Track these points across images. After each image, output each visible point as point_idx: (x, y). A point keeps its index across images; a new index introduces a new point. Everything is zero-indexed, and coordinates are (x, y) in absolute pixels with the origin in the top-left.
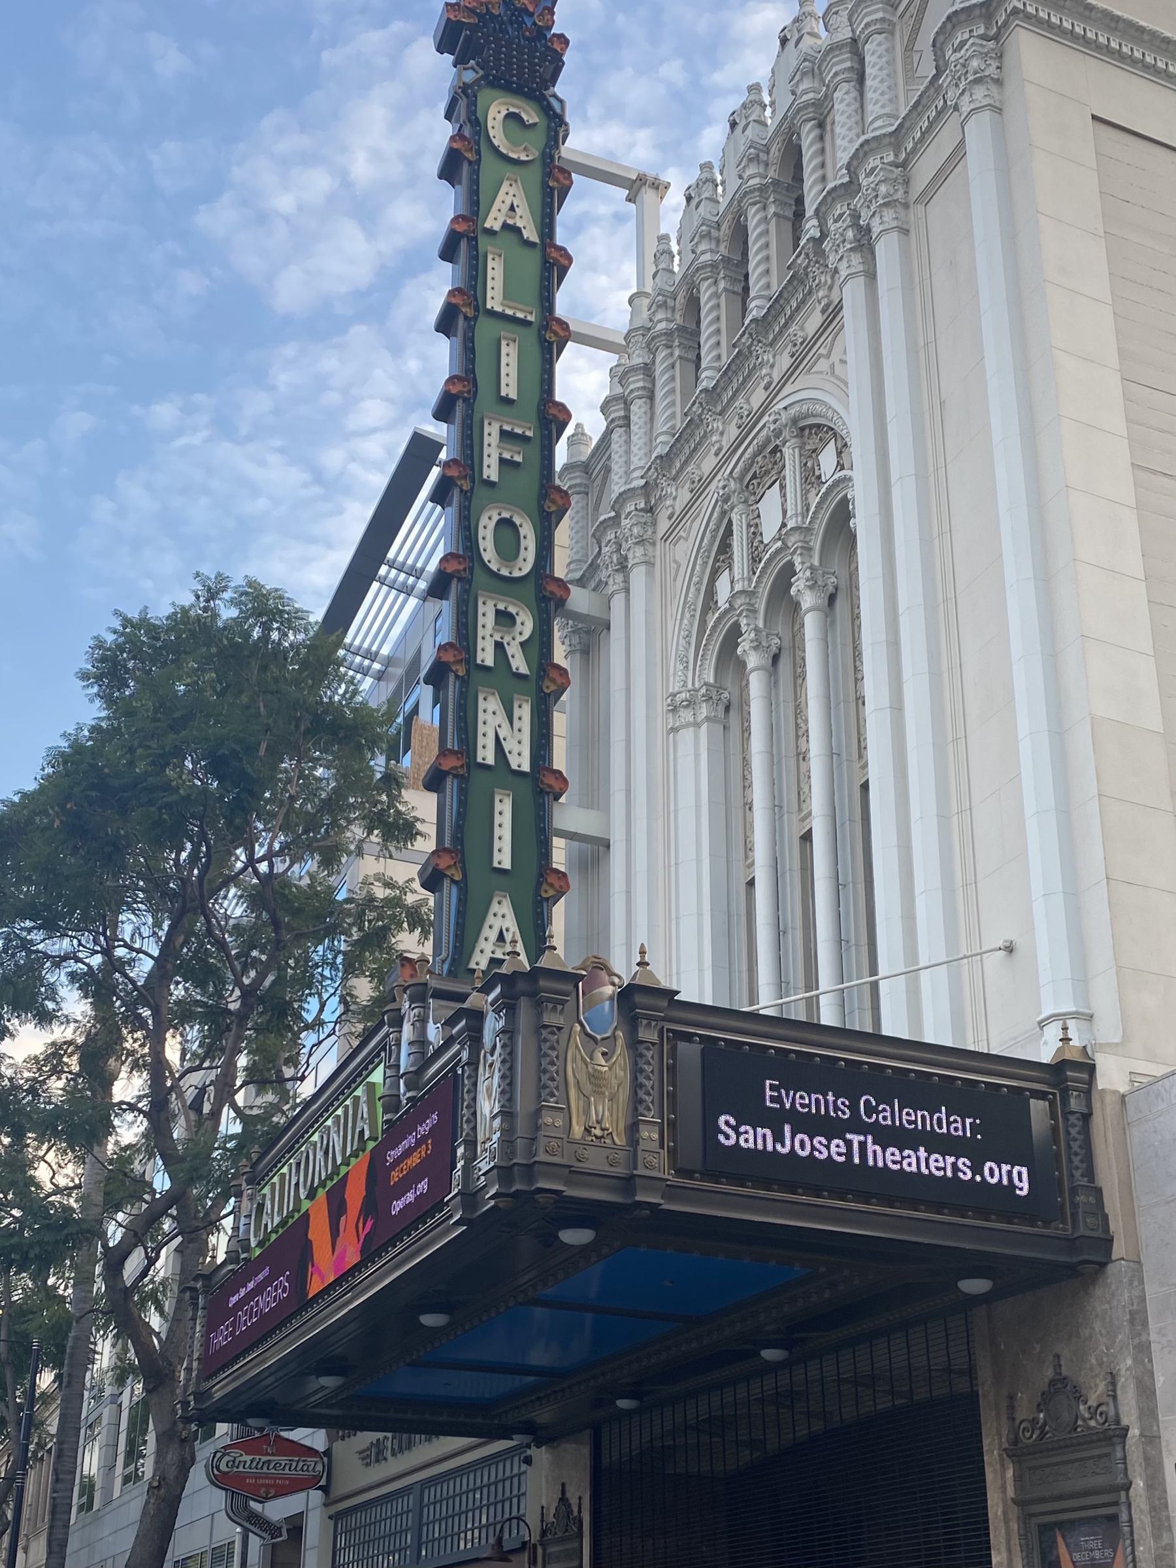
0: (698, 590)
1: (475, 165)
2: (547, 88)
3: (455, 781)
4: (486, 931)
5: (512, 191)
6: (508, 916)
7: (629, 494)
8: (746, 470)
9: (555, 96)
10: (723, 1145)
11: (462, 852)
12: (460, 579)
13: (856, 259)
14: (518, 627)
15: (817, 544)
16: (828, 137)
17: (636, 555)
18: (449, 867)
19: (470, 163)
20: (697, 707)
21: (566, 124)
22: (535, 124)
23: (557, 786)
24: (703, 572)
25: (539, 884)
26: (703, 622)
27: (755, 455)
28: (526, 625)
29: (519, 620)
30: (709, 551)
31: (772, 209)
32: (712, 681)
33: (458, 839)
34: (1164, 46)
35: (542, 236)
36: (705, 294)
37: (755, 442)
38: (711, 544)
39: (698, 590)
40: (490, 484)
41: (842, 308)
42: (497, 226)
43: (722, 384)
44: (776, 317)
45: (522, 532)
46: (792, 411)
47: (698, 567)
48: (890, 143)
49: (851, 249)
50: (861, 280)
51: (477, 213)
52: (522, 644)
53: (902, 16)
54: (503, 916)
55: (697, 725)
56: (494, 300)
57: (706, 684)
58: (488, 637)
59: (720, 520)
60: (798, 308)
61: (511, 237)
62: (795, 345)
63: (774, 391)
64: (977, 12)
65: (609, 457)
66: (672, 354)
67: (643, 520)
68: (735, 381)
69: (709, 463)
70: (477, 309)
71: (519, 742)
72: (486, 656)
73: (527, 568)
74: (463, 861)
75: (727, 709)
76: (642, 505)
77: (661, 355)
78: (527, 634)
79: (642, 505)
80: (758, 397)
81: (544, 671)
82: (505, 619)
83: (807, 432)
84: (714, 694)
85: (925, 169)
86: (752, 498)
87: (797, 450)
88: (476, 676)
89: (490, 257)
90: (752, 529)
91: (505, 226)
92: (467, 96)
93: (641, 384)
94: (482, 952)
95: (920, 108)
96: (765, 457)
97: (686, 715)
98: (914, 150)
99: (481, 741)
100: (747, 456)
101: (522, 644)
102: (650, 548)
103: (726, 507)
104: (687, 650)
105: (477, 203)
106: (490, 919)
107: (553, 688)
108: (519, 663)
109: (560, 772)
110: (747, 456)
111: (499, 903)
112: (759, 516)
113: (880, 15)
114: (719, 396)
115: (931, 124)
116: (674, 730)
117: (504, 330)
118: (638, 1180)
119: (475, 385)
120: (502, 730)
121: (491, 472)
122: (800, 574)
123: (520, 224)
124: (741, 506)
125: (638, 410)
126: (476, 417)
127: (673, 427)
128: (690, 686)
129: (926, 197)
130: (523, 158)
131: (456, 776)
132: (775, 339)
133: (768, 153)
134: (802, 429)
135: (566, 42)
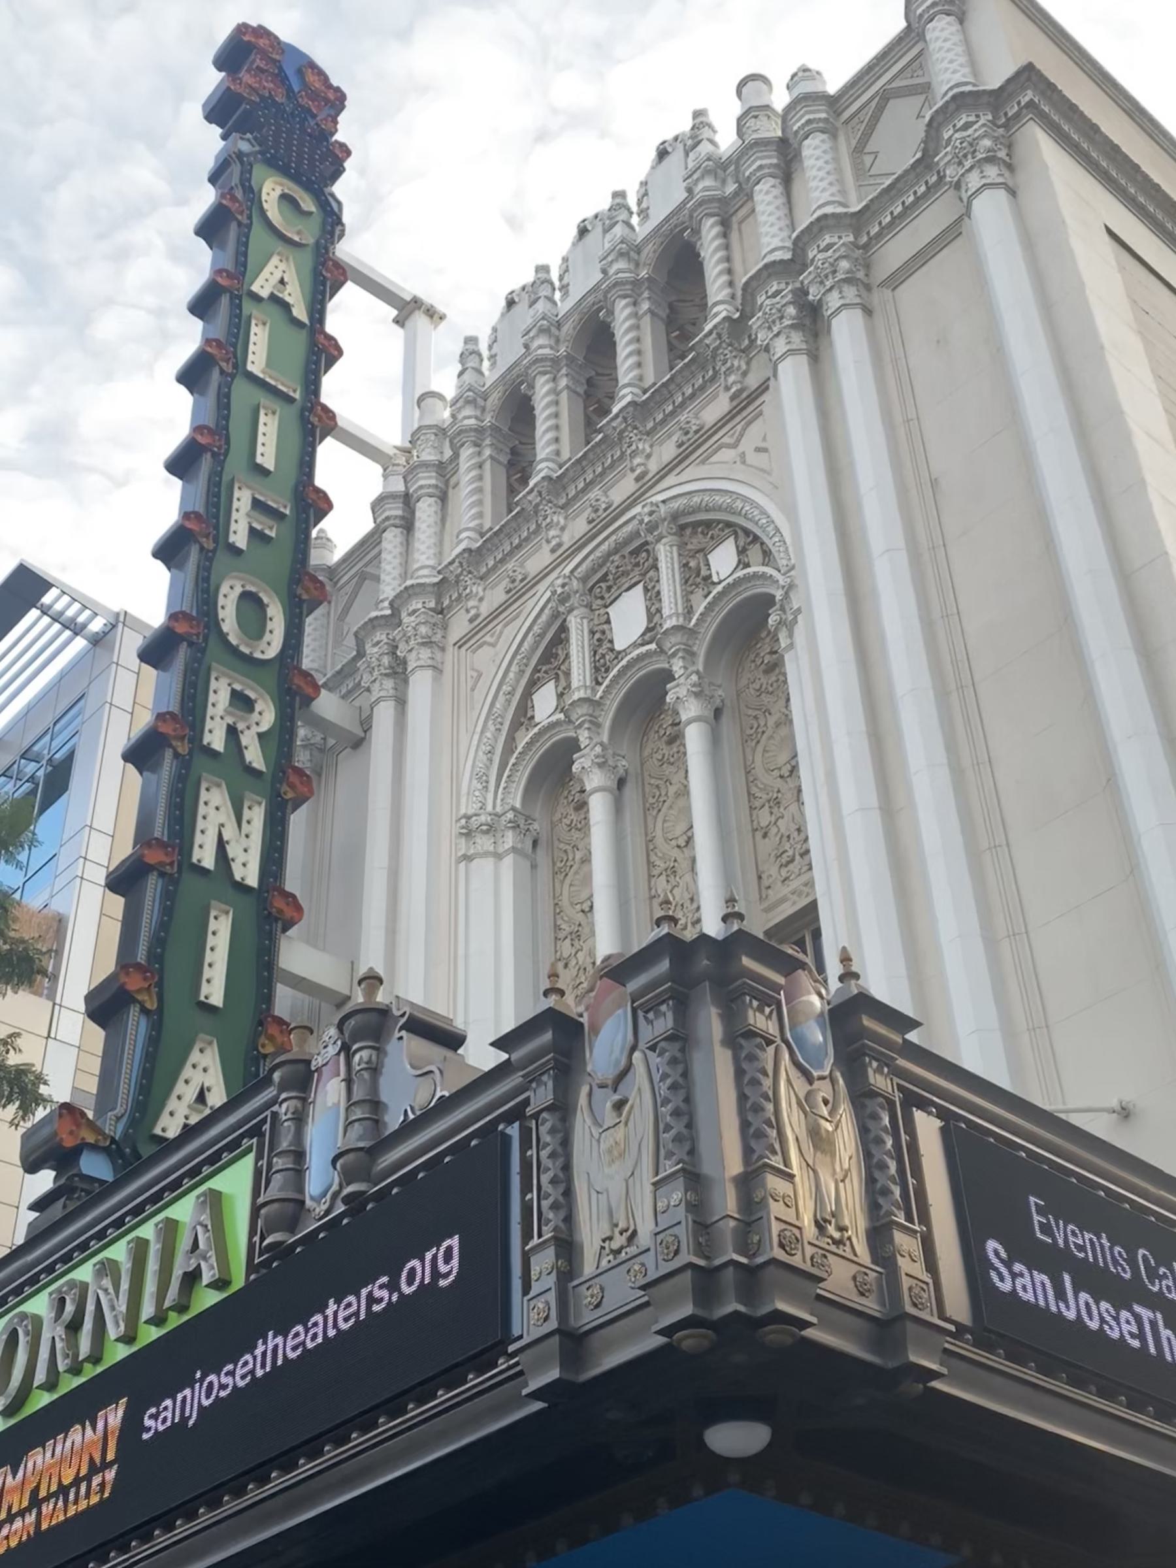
0: (509, 702)
1: (245, 231)
2: (326, 186)
3: (160, 882)
4: (180, 1087)
5: (282, 266)
6: (211, 1071)
7: (417, 590)
8: (594, 570)
9: (333, 195)
10: (1050, 1278)
11: (161, 971)
12: (191, 644)
13: (797, 338)
14: (255, 716)
15: (701, 650)
16: (734, 236)
17: (417, 657)
18: (139, 991)
19: (240, 224)
20: (499, 835)
21: (343, 225)
22: (310, 213)
23: (289, 913)
24: (518, 681)
25: (256, 1035)
26: (511, 740)
27: (610, 554)
28: (266, 716)
29: (258, 707)
30: (528, 658)
31: (645, 306)
32: (518, 805)
33: (157, 956)
34: (1153, 192)
35: (311, 317)
36: (542, 392)
37: (614, 537)
38: (534, 649)
39: (509, 702)
40: (237, 552)
41: (767, 388)
42: (264, 294)
43: (571, 474)
44: (660, 404)
45: (270, 612)
46: (675, 505)
47: (511, 675)
48: (850, 225)
49: (792, 326)
50: (804, 359)
51: (244, 274)
52: (261, 736)
53: (847, 122)
54: (205, 1070)
55: (498, 856)
56: (256, 362)
57: (513, 809)
58: (218, 719)
59: (549, 624)
60: (693, 396)
61: (275, 310)
62: (687, 433)
63: (646, 483)
64: (985, 99)
65: (380, 553)
66: (479, 454)
67: (433, 621)
68: (590, 471)
69: (537, 560)
70: (235, 366)
71: (246, 851)
72: (216, 739)
73: (272, 652)
74: (160, 985)
75: (535, 843)
76: (432, 605)
77: (466, 452)
78: (265, 727)
79: (432, 605)
80: (624, 488)
81: (284, 773)
82: (242, 702)
83: (688, 531)
84: (522, 822)
85: (895, 252)
86: (599, 602)
87: (675, 548)
88: (199, 761)
89: (253, 322)
90: (597, 636)
91: (273, 298)
92: (242, 163)
93: (433, 482)
94: (171, 1114)
95: (894, 192)
96: (624, 557)
97: (484, 843)
98: (879, 235)
99: (198, 838)
100: (598, 553)
101: (261, 736)
102: (438, 655)
103: (562, 609)
104: (488, 768)
105: (245, 265)
106: (187, 1072)
107: (290, 795)
108: (254, 756)
109: (294, 896)
110: (598, 553)
111: (201, 1051)
112: (608, 622)
113: (823, 115)
114: (564, 488)
115: (918, 199)
116: (468, 858)
117: (264, 399)
118: (910, 1326)
119: (228, 442)
120: (228, 832)
121: (239, 537)
122: (682, 680)
123: (288, 299)
124: (583, 610)
125: (426, 511)
126: (226, 478)
127: (481, 525)
128: (489, 808)
129: (895, 280)
130: (296, 238)
131: (162, 875)
132: (654, 429)
133: (639, 253)
134: (683, 528)
135: (348, 153)
